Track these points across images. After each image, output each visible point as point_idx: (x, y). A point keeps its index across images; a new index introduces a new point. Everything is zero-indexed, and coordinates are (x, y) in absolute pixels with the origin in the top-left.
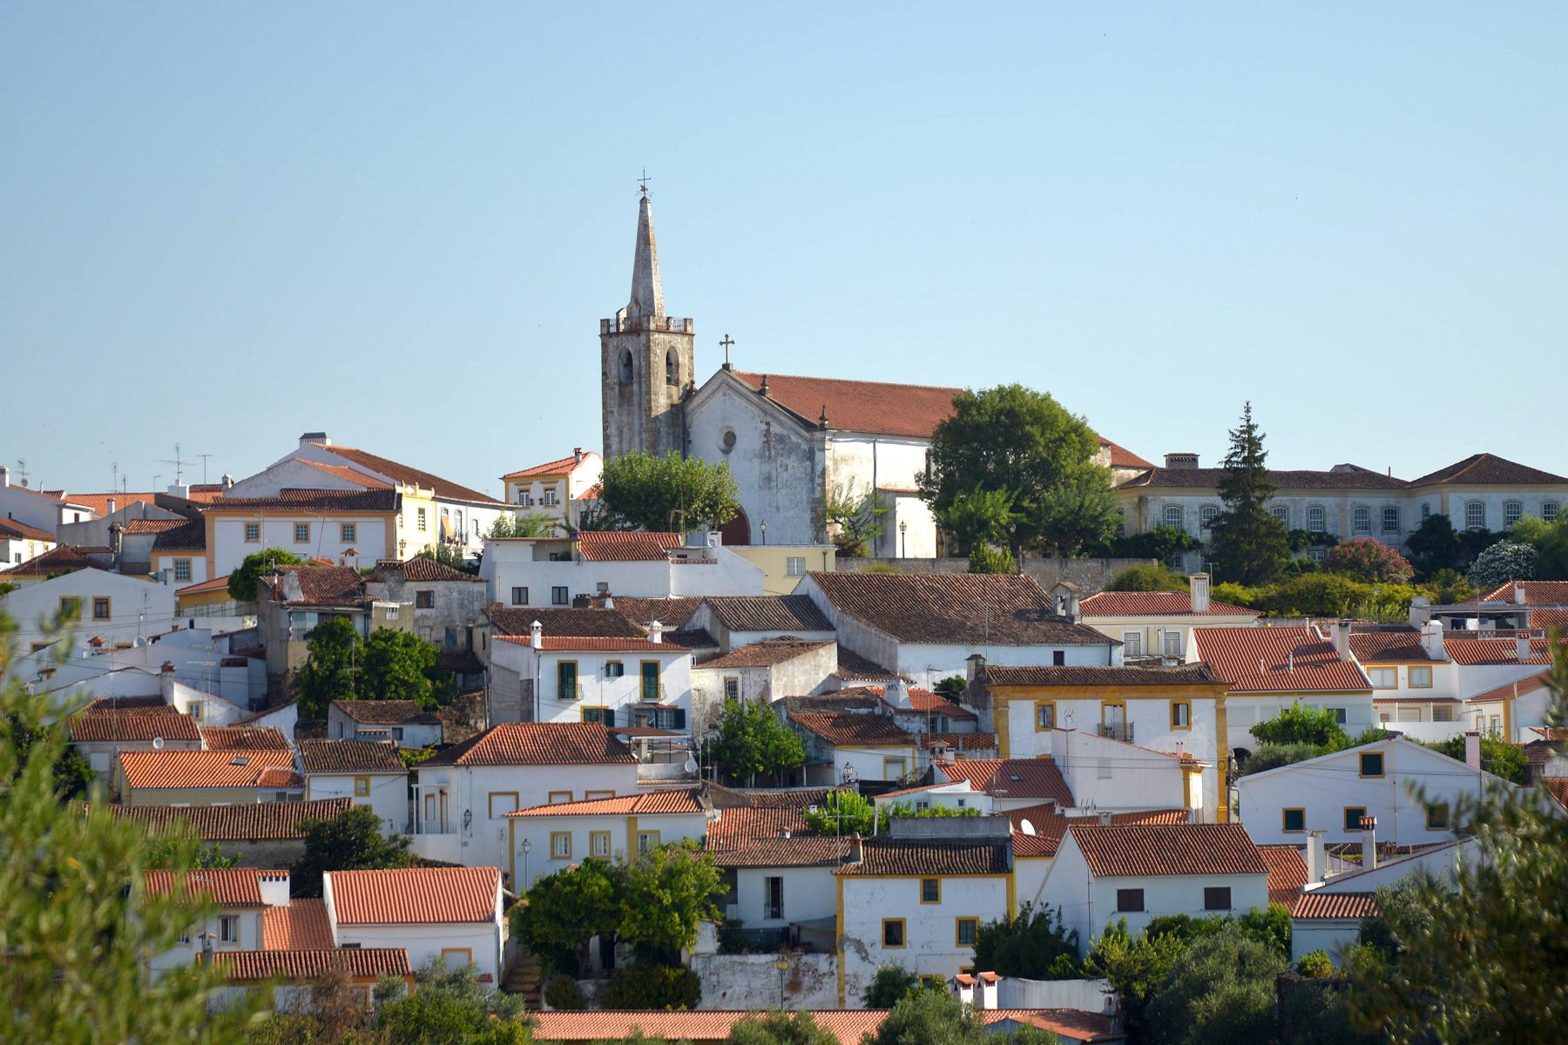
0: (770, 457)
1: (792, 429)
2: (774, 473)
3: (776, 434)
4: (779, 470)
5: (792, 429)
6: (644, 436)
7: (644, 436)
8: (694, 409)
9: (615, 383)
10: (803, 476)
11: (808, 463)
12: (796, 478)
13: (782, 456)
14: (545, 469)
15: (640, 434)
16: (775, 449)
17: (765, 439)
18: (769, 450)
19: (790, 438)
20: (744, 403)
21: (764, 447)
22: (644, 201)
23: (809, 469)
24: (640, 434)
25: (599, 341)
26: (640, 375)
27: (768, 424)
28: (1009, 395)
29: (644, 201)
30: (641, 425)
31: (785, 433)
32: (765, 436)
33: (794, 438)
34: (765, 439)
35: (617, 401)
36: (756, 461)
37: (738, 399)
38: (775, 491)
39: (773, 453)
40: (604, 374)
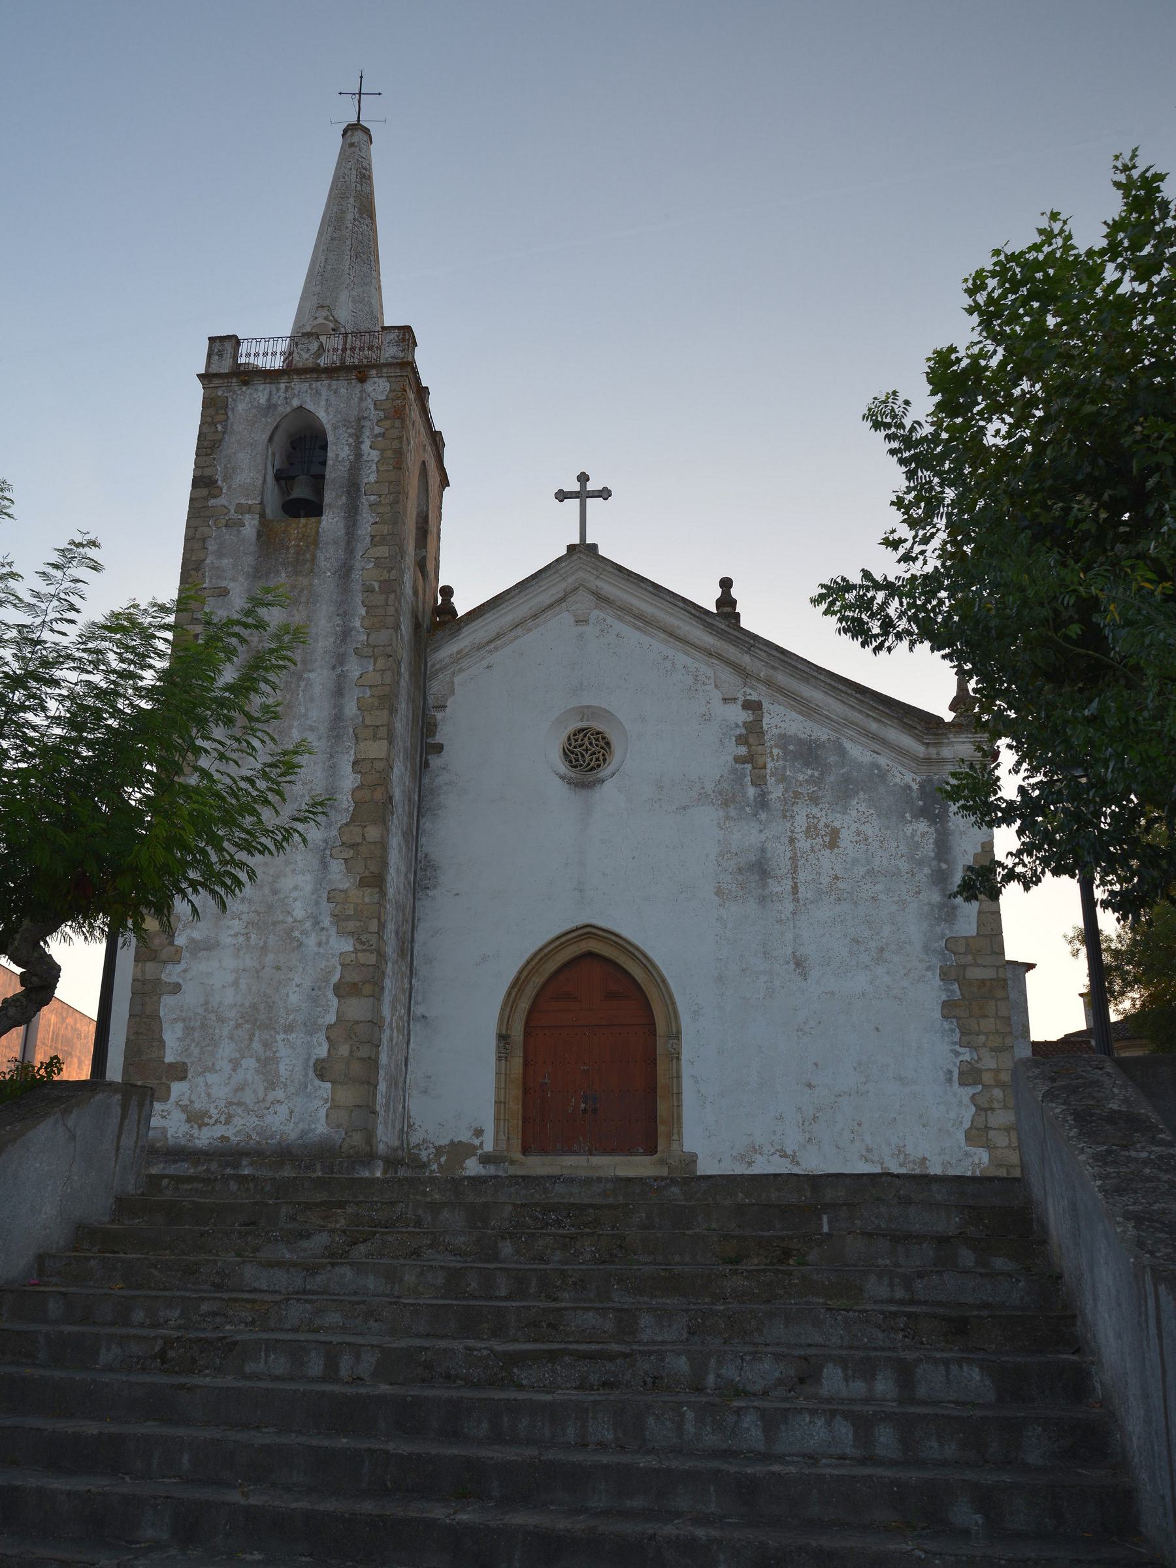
0: (762, 802)
1: (849, 723)
2: (780, 856)
3: (784, 740)
4: (803, 844)
5: (849, 723)
6: (354, 668)
7: (354, 668)
8: (460, 656)
9: (242, 509)
10: (904, 865)
11: (922, 826)
12: (870, 872)
13: (815, 800)
15: (341, 659)
16: (783, 779)
17: (743, 750)
18: (759, 781)
19: (841, 751)
20: (657, 646)
21: (739, 779)
22: (361, 77)
23: (928, 848)
24: (341, 659)
25: (197, 392)
26: (353, 488)
27: (752, 706)
28: (1066, 1036)
29: (361, 77)
30: (345, 634)
31: (822, 734)
32: (741, 740)
33: (859, 752)
34: (743, 750)
35: (249, 561)
36: (708, 816)
37: (632, 636)
38: (790, 907)
39: (776, 792)
40: (203, 483)
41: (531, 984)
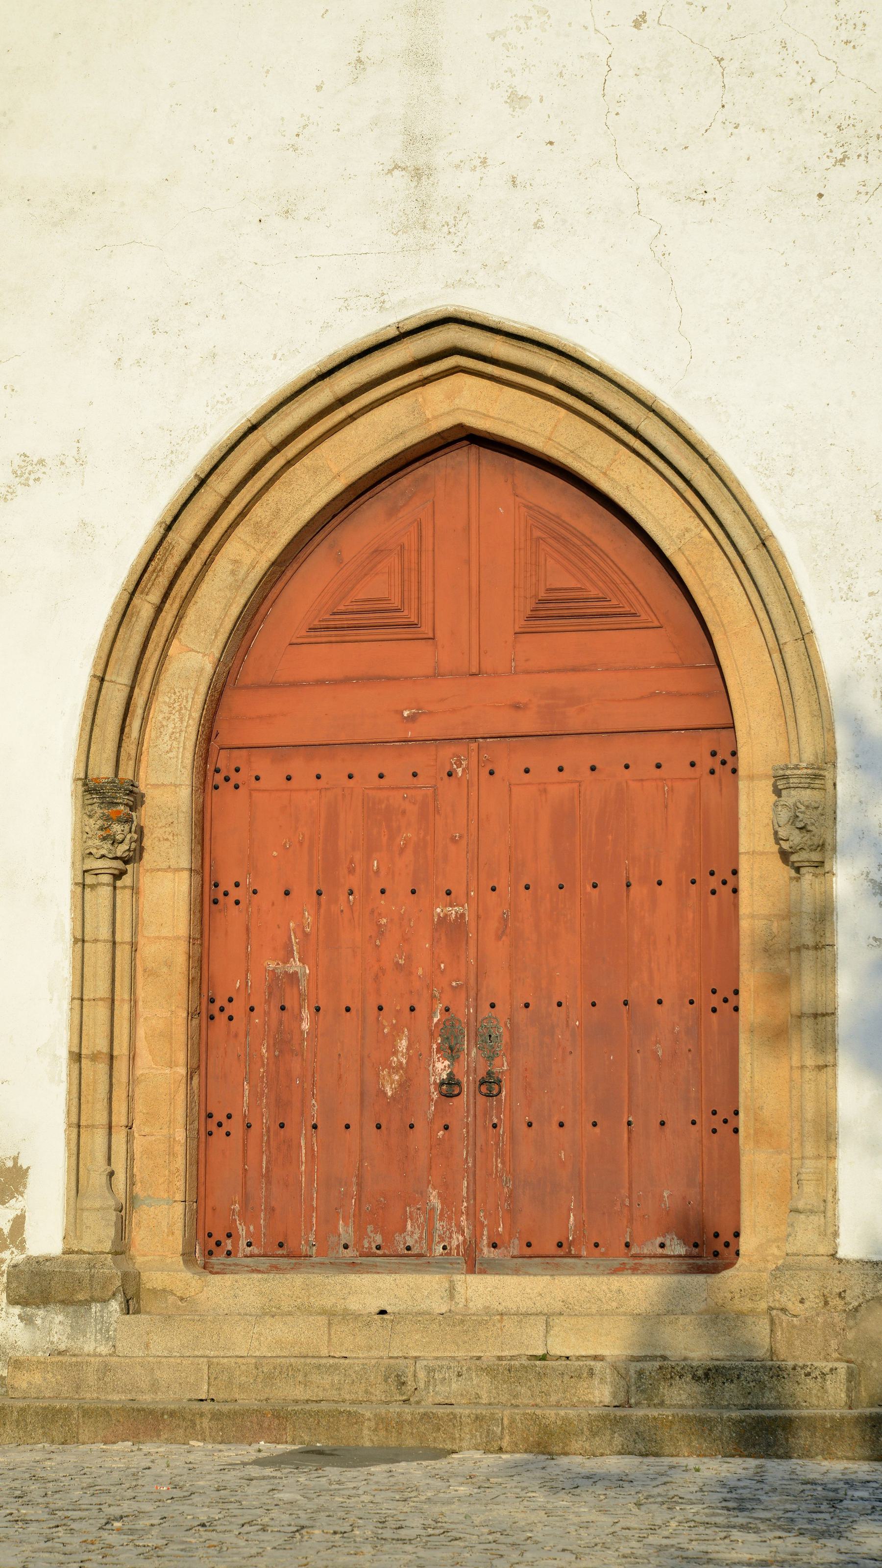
14: (99, 955)
41: (222, 565)
